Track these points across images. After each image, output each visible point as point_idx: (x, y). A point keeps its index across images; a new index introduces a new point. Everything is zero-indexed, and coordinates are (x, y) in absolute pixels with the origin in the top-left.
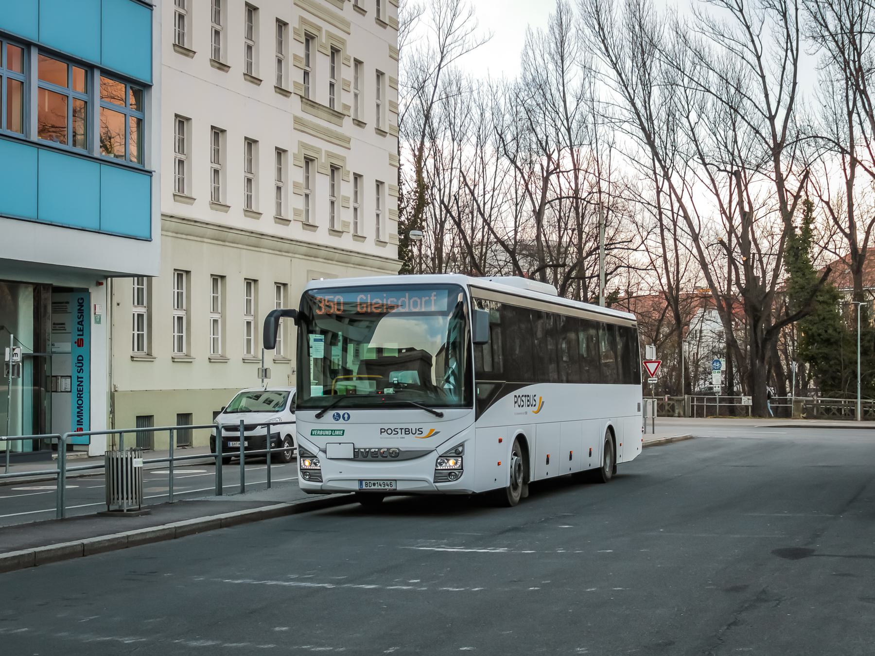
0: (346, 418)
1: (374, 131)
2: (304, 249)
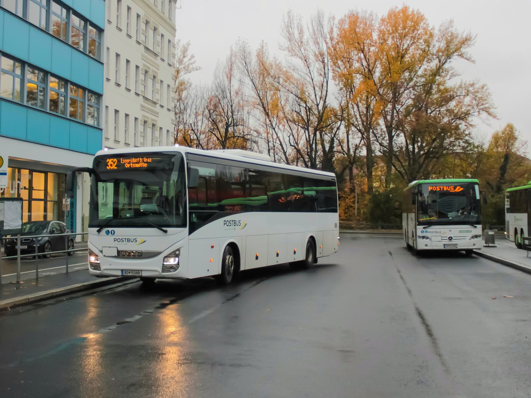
0: (113, 234)
1: (124, 89)
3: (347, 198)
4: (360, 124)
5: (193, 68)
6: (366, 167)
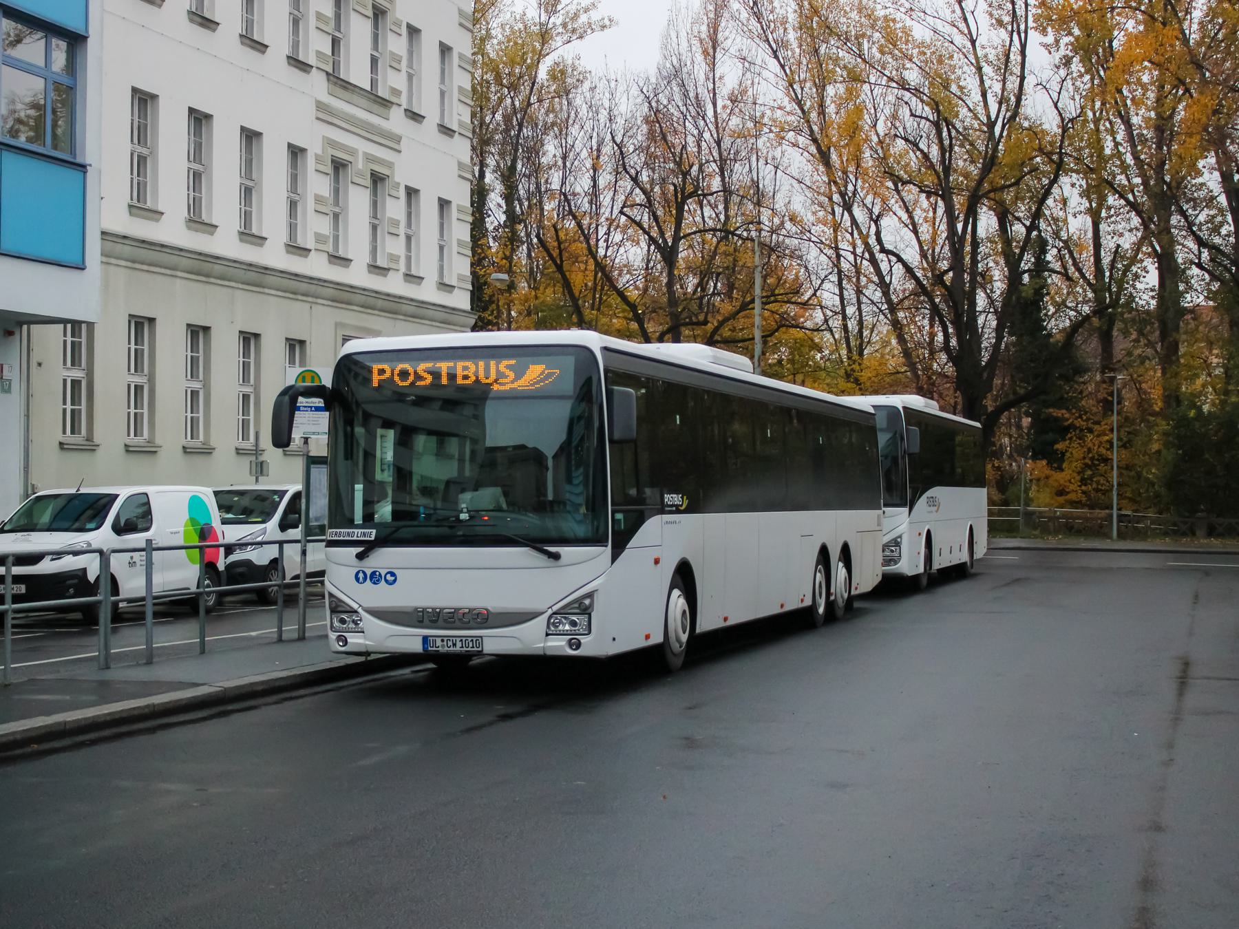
2: (329, 292)
3: (1091, 431)
4: (1137, 185)
5: (590, 24)
6: (1156, 325)
